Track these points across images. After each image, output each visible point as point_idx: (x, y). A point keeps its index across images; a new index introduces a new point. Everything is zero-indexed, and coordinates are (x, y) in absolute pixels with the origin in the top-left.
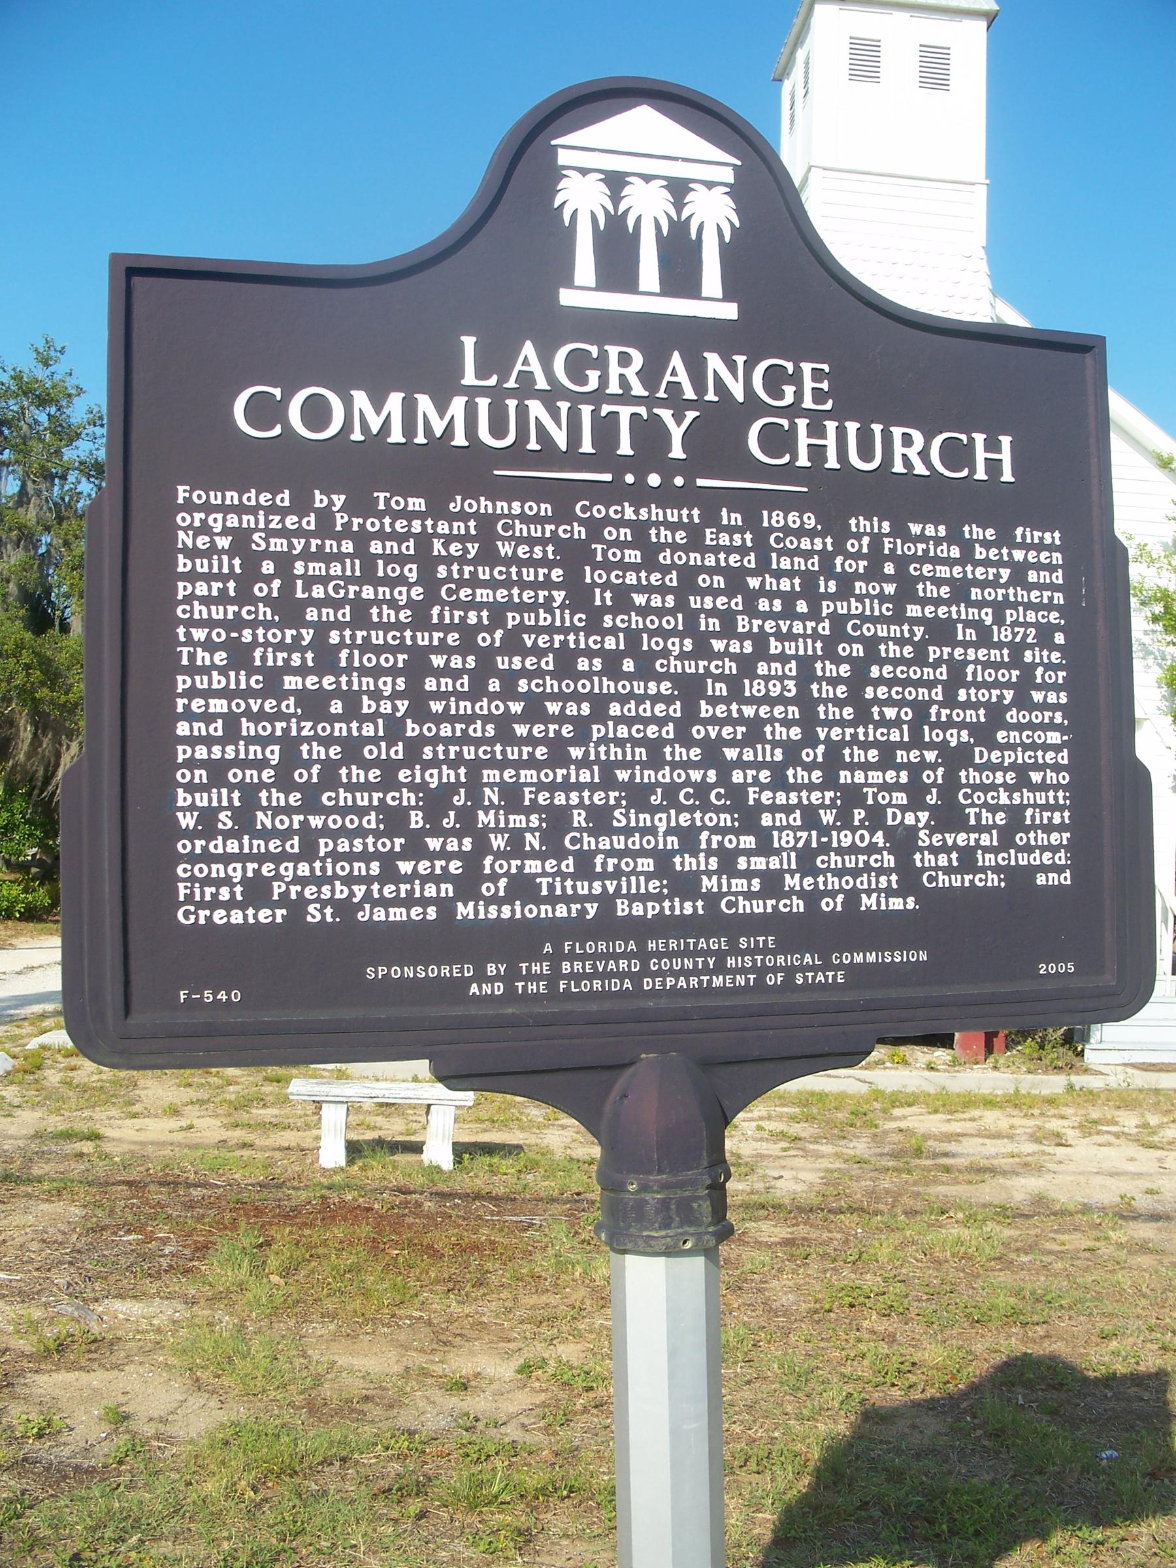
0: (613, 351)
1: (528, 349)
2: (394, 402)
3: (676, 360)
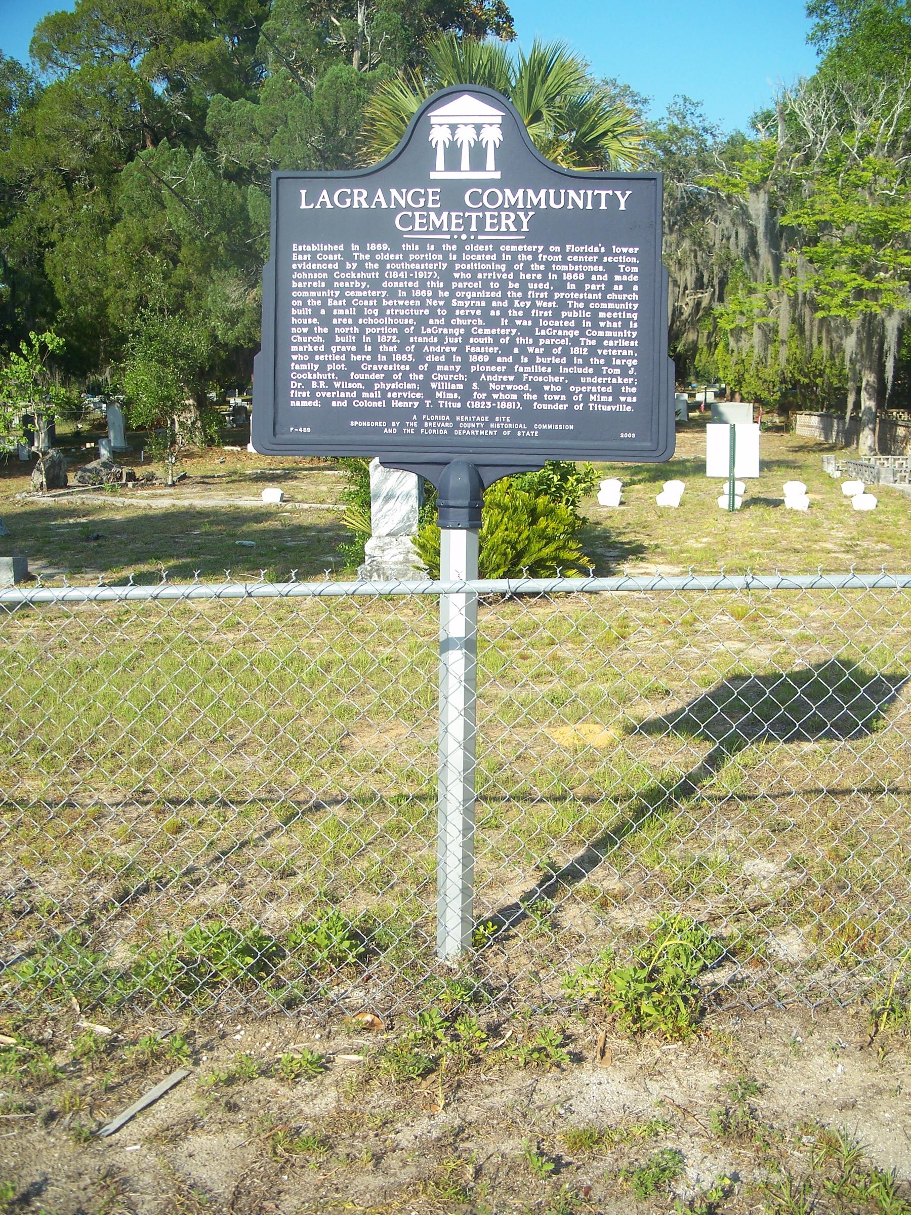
0: (356, 191)
1: (325, 193)
2: (520, 192)
3: (380, 192)
